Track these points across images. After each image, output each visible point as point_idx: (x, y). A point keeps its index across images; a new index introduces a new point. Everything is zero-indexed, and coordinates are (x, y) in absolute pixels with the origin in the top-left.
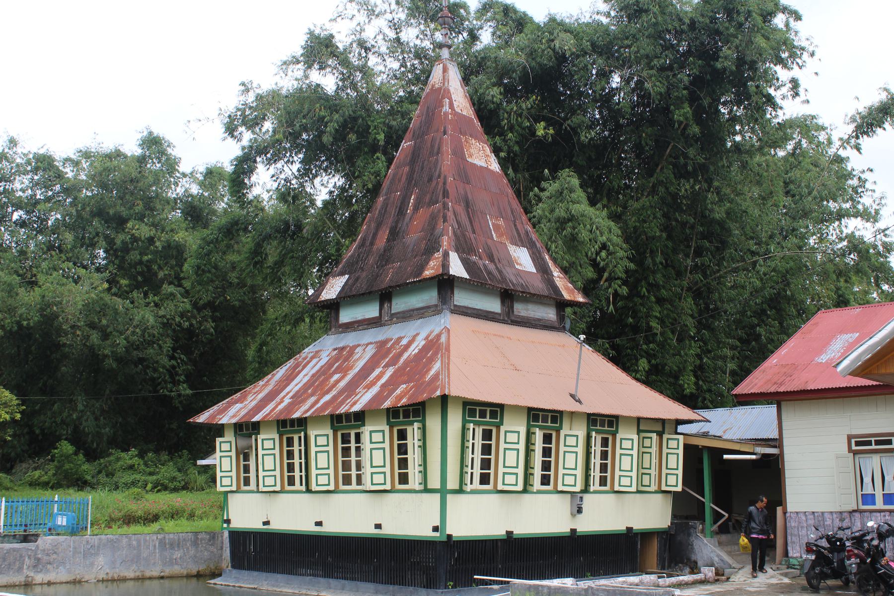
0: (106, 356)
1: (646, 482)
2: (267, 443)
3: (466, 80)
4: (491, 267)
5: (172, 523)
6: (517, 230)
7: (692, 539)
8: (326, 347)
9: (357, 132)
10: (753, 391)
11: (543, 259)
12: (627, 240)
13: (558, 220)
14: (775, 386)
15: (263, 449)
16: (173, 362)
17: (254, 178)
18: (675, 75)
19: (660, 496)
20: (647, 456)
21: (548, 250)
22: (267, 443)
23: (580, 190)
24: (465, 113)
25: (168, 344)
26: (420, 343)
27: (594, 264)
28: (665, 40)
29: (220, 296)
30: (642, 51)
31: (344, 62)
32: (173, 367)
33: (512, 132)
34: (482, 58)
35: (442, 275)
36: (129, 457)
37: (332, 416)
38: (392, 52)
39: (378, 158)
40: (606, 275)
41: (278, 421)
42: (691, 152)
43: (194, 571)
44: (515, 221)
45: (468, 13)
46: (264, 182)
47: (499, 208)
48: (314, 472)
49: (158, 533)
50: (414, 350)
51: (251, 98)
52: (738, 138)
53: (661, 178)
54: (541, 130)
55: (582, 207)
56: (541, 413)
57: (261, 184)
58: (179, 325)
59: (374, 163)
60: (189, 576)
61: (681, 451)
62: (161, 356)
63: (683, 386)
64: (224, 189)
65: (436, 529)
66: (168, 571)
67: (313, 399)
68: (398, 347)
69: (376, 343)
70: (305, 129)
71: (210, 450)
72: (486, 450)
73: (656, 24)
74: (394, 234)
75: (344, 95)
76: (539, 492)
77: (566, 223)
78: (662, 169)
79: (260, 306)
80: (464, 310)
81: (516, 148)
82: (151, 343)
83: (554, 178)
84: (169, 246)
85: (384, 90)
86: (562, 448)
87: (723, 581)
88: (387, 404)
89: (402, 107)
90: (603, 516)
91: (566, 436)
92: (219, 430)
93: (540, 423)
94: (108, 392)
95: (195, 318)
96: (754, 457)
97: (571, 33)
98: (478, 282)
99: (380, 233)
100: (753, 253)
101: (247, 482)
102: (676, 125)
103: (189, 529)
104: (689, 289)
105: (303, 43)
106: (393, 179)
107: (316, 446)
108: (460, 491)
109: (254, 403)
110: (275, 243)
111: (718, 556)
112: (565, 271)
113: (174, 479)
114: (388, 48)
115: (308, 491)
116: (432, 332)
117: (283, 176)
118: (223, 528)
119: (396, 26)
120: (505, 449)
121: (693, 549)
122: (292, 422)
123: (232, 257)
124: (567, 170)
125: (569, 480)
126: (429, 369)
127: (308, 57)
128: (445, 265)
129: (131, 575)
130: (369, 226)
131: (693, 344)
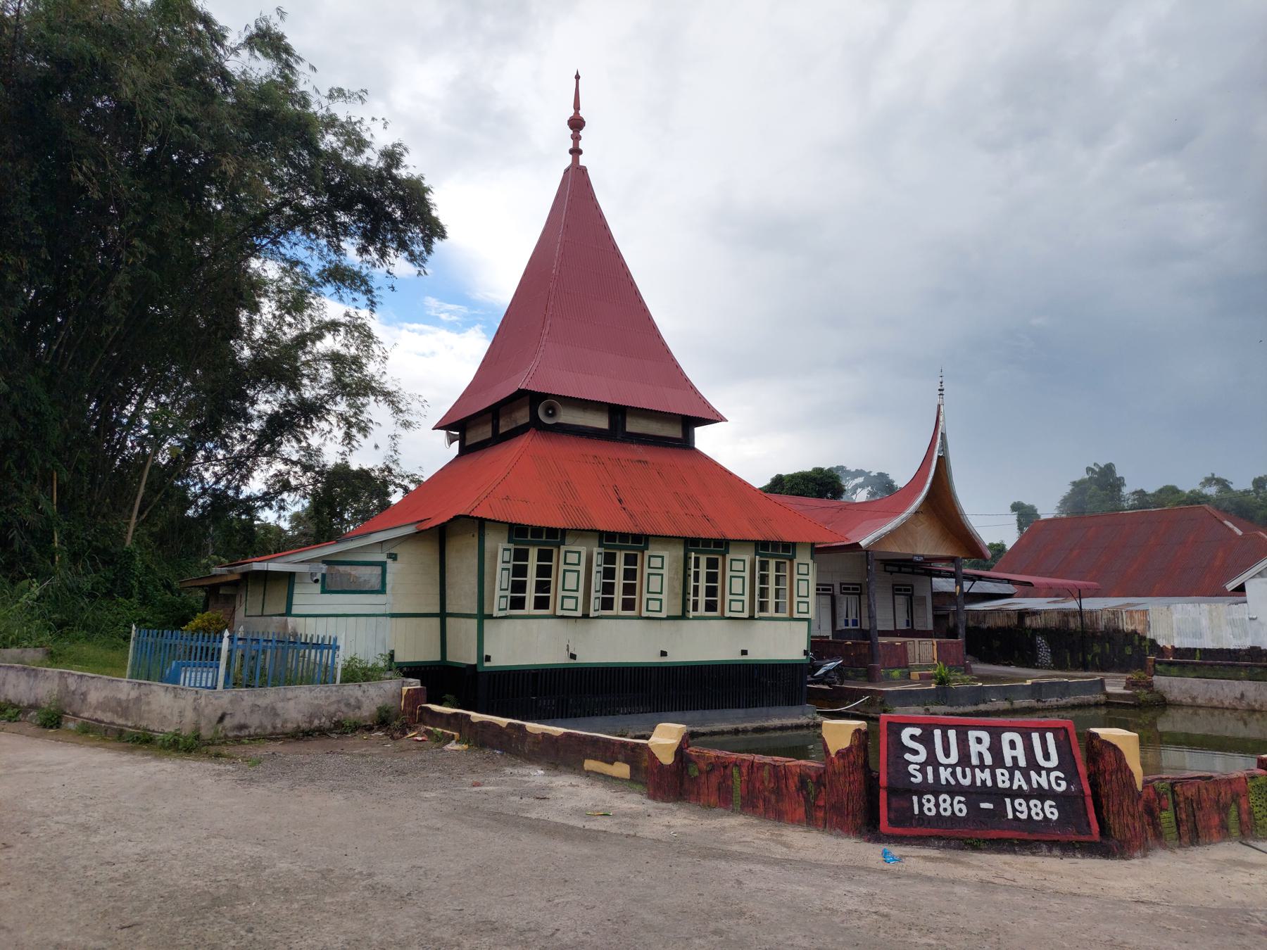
72: (712, 577)
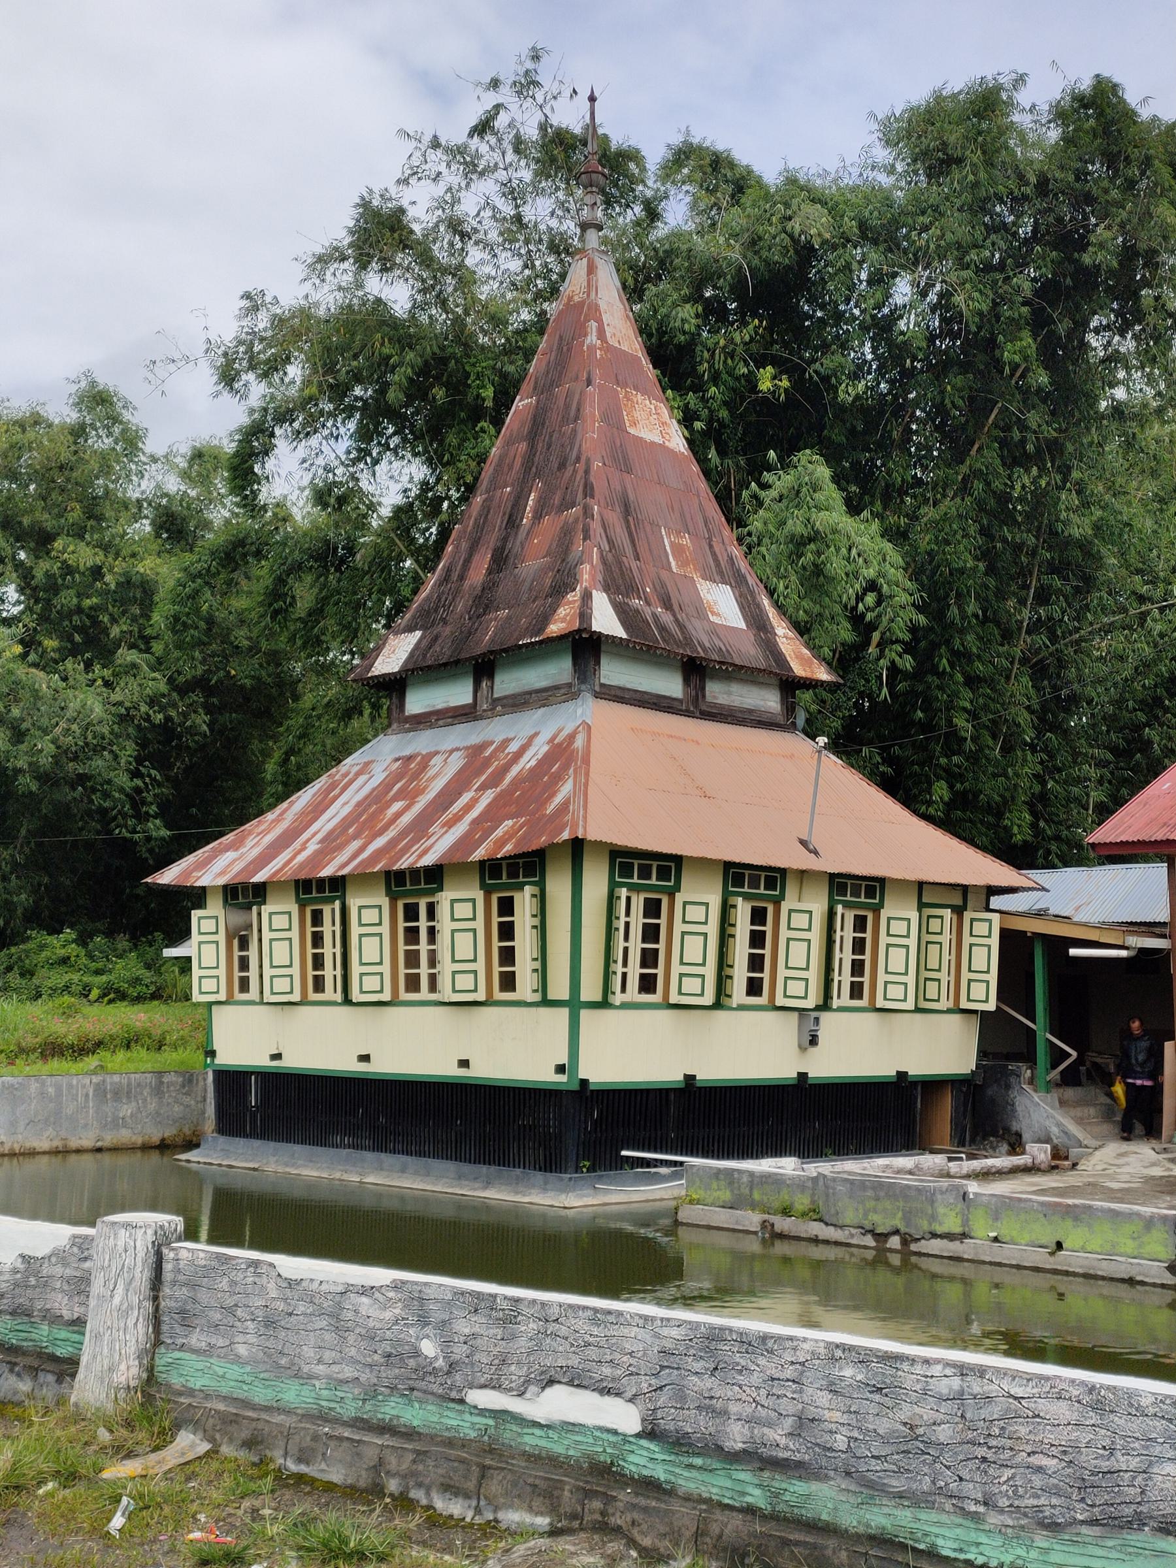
0: (18, 771)
1: (932, 992)
2: (279, 918)
3: (633, 292)
4: (667, 618)
5: (121, 1055)
6: (714, 554)
7: (1013, 1093)
8: (378, 758)
9: (447, 385)
10: (1124, 838)
11: (759, 606)
12: (915, 576)
13: (792, 538)
14: (1165, 830)
15: (271, 930)
16: (138, 782)
17: (271, 464)
18: (1007, 279)
19: (957, 1017)
20: (933, 950)
21: (771, 592)
22: (279, 918)
23: (833, 486)
24: (625, 347)
25: (128, 750)
26: (540, 748)
27: (856, 620)
28: (992, 214)
29: (218, 669)
30: (949, 236)
31: (426, 259)
32: (138, 790)
33: (716, 385)
34: (665, 251)
35: (579, 631)
36: (62, 943)
37: (388, 874)
38: (509, 238)
39: (483, 431)
40: (876, 636)
41: (297, 882)
42: (1033, 418)
43: (156, 1140)
44: (710, 539)
45: (643, 169)
46: (291, 476)
47: (682, 515)
48: (356, 969)
49: (94, 1072)
50: (528, 761)
51: (262, 322)
52: (1120, 393)
53: (978, 465)
54: (766, 379)
55: (832, 513)
56: (747, 872)
57: (283, 474)
58: (148, 718)
59: (476, 438)
60: (146, 1148)
61: (995, 942)
62: (116, 771)
63: (1011, 828)
64: (220, 484)
65: (560, 1069)
66: (109, 1139)
67: (355, 845)
68: (502, 755)
69: (467, 748)
70: (358, 378)
71: (181, 933)
72: (651, 933)
73: (976, 185)
74: (500, 560)
75: (424, 319)
76: (742, 1008)
77: (805, 545)
78: (980, 449)
79: (288, 688)
80: (619, 693)
81: (724, 414)
82: (98, 750)
83: (785, 465)
84: (129, 582)
85: (492, 309)
86: (784, 933)
87: (1065, 1170)
88: (479, 854)
89: (524, 340)
90: (855, 1050)
91: (790, 911)
92: (198, 897)
93: (746, 890)
94: (23, 832)
95: (174, 706)
96: (1124, 953)
97: (824, 203)
98: (642, 646)
99: (476, 558)
100: (1142, 599)
101: (244, 985)
102: (1007, 370)
103: (149, 1066)
104: (1024, 661)
105: (351, 223)
106: (500, 464)
107: (361, 925)
108: (604, 1004)
109: (255, 852)
110: (309, 579)
111: (1059, 1125)
112: (802, 629)
113: (137, 981)
114: (501, 234)
115: (347, 1001)
116: (560, 731)
117: (320, 461)
118: (206, 1066)
119: (513, 193)
120: (683, 933)
121: (1014, 1111)
122: (321, 881)
123: (239, 603)
124: (808, 451)
125: (796, 988)
126: (554, 794)
127: (360, 248)
128: (585, 614)
129: (45, 1145)
130: (457, 547)
131: (1029, 757)
